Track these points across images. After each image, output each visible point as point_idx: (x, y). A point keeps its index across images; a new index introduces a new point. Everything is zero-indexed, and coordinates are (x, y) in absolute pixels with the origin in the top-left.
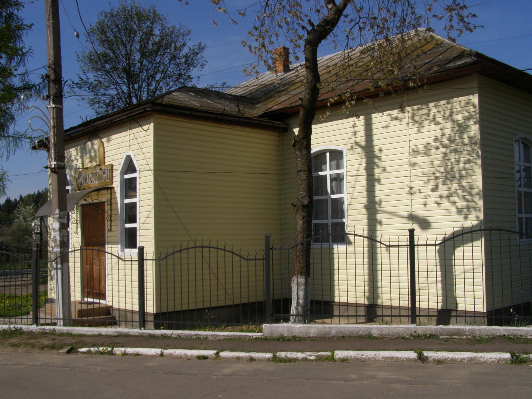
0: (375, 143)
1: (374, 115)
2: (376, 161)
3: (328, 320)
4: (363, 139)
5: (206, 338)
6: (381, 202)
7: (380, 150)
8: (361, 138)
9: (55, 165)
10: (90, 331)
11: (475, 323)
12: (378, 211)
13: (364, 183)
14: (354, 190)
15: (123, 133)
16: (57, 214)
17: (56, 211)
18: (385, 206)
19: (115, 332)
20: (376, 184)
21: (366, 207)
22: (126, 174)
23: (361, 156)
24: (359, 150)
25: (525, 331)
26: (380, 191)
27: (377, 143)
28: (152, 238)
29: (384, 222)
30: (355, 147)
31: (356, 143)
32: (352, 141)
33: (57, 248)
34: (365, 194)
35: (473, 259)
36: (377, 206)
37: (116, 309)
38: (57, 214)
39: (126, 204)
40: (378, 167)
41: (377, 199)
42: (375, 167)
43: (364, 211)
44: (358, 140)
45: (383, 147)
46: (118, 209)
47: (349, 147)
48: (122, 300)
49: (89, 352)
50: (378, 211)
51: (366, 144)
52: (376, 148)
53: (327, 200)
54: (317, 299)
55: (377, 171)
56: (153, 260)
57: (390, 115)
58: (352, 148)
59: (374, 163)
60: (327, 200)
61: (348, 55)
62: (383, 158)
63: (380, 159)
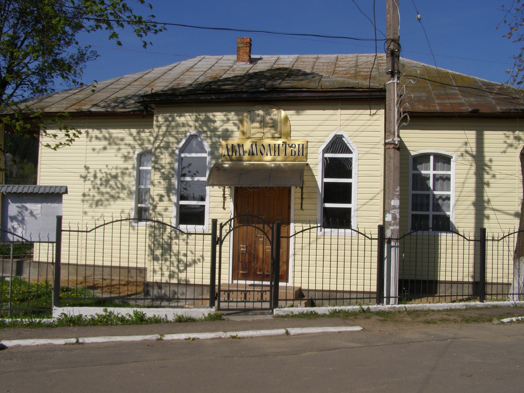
0: (486, 154)
1: (486, 132)
2: (486, 168)
3: (430, 299)
4: (474, 149)
5: (428, 312)
6: (489, 201)
7: (491, 161)
8: (472, 147)
9: (398, 141)
10: (440, 307)
11: (336, 305)
12: (486, 208)
13: (473, 185)
14: (462, 190)
15: (326, 111)
16: (397, 191)
17: (397, 188)
18: (494, 204)
19: (463, 306)
20: (485, 186)
21: (474, 204)
22: (327, 153)
23: (471, 163)
24: (470, 158)
25: (398, 308)
26: (488, 193)
27: (488, 155)
28: (380, 220)
29: (491, 217)
30: (465, 154)
31: (467, 152)
32: (463, 149)
33: (397, 226)
34: (474, 194)
35: (345, 250)
36: (486, 204)
37: (305, 290)
38: (397, 191)
39: (325, 182)
40: (488, 173)
41: (486, 198)
42: (485, 173)
43: (472, 207)
44: (469, 149)
45: (494, 159)
46: (317, 187)
47: (459, 153)
48: (312, 280)
49: (511, 322)
50: (486, 208)
51: (477, 154)
52: (487, 159)
53: (428, 196)
54: (423, 279)
55: (487, 178)
56: (487, 240)
57: (505, 134)
58: (462, 155)
59: (484, 170)
60: (428, 196)
61: (315, 62)
62: (493, 168)
63: (490, 167)
